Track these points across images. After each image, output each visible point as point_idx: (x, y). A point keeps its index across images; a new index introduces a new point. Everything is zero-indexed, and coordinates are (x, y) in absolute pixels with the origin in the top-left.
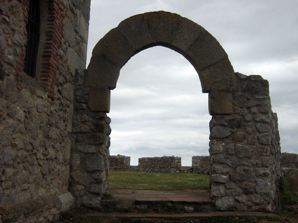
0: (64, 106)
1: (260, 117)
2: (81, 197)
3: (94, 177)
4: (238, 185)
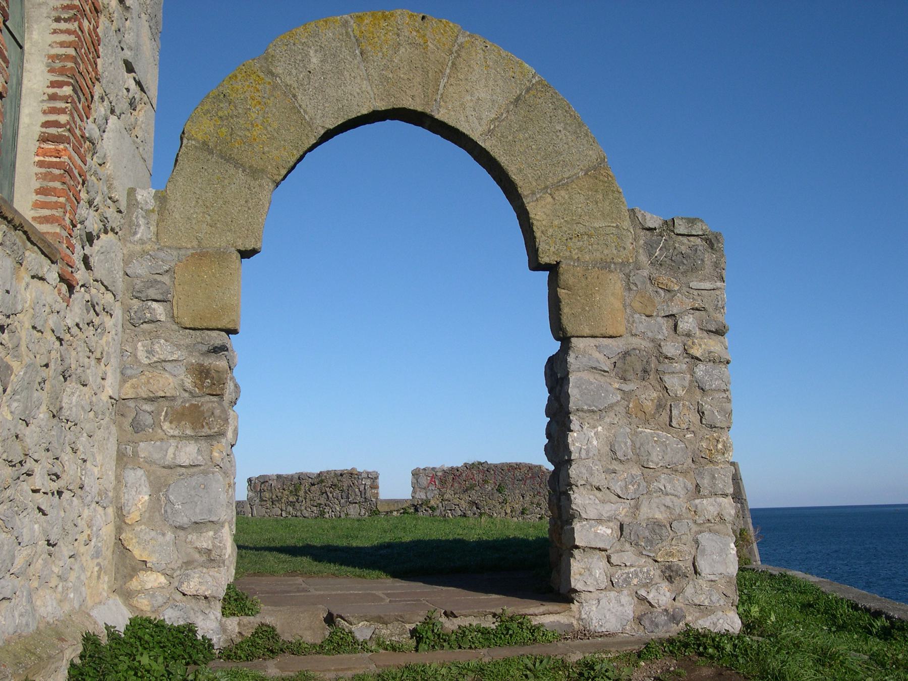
3: (198, 545)
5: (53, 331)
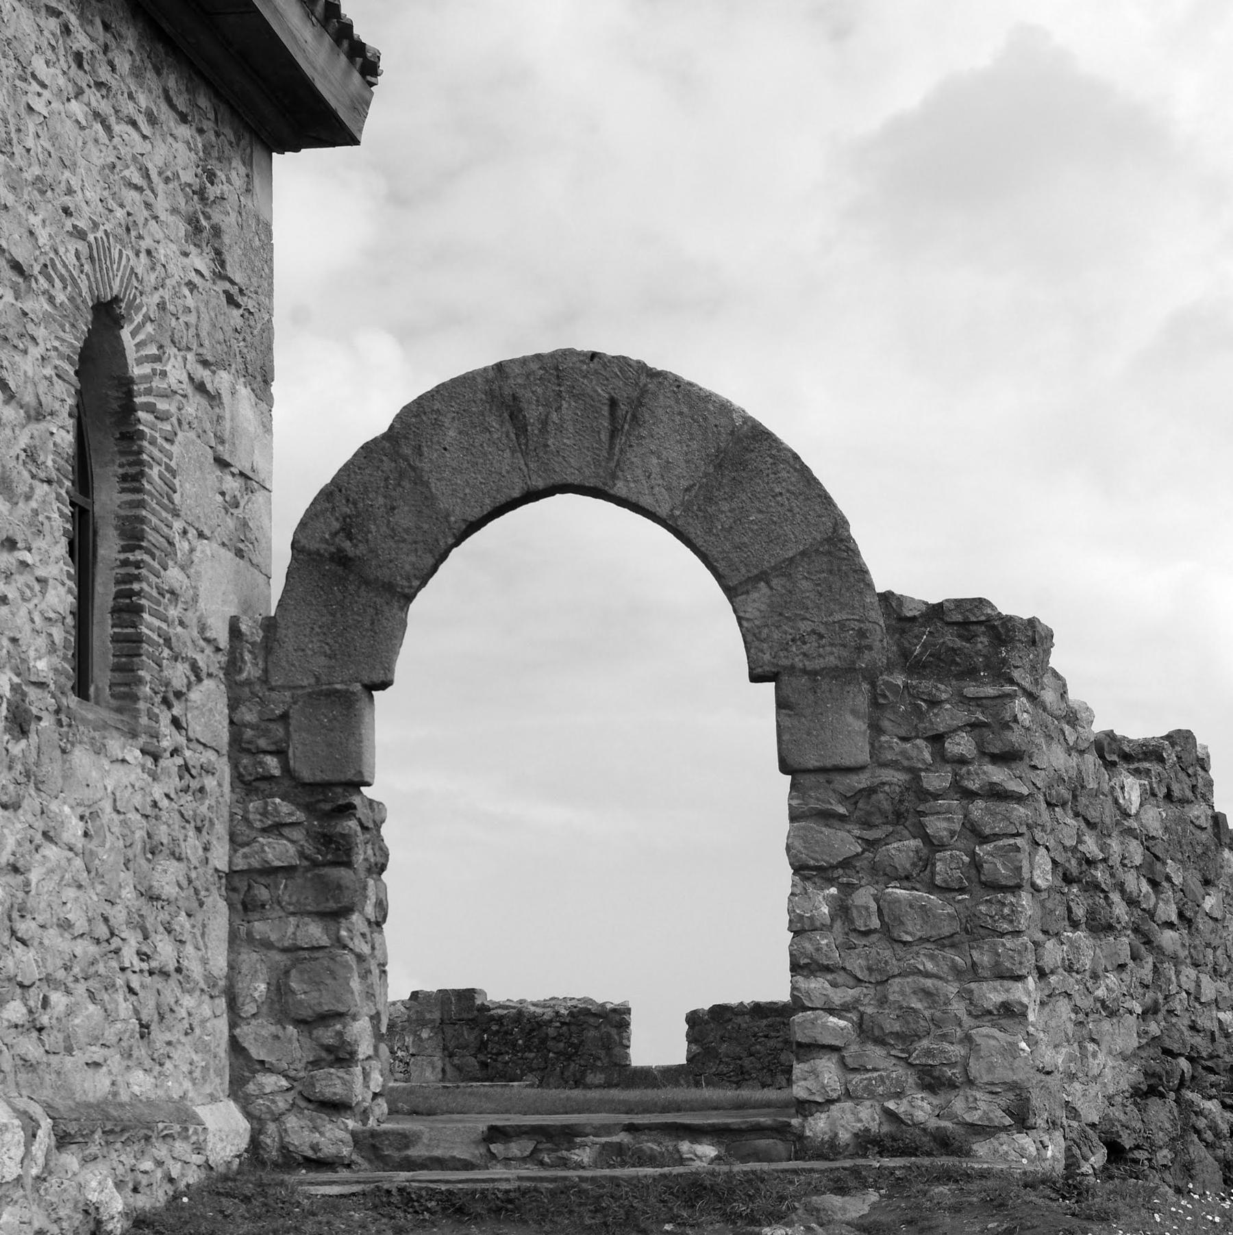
0: (193, 772)
1: (985, 773)
2: (277, 1118)
4: (892, 1052)
5: (137, 810)
